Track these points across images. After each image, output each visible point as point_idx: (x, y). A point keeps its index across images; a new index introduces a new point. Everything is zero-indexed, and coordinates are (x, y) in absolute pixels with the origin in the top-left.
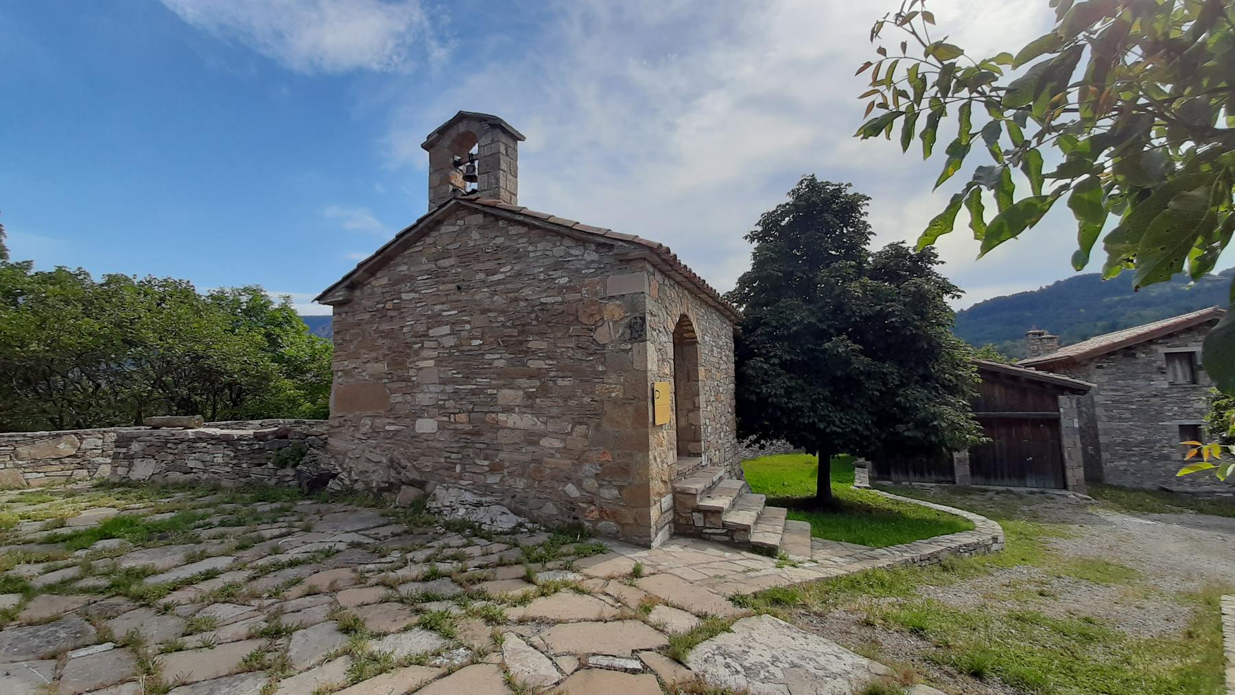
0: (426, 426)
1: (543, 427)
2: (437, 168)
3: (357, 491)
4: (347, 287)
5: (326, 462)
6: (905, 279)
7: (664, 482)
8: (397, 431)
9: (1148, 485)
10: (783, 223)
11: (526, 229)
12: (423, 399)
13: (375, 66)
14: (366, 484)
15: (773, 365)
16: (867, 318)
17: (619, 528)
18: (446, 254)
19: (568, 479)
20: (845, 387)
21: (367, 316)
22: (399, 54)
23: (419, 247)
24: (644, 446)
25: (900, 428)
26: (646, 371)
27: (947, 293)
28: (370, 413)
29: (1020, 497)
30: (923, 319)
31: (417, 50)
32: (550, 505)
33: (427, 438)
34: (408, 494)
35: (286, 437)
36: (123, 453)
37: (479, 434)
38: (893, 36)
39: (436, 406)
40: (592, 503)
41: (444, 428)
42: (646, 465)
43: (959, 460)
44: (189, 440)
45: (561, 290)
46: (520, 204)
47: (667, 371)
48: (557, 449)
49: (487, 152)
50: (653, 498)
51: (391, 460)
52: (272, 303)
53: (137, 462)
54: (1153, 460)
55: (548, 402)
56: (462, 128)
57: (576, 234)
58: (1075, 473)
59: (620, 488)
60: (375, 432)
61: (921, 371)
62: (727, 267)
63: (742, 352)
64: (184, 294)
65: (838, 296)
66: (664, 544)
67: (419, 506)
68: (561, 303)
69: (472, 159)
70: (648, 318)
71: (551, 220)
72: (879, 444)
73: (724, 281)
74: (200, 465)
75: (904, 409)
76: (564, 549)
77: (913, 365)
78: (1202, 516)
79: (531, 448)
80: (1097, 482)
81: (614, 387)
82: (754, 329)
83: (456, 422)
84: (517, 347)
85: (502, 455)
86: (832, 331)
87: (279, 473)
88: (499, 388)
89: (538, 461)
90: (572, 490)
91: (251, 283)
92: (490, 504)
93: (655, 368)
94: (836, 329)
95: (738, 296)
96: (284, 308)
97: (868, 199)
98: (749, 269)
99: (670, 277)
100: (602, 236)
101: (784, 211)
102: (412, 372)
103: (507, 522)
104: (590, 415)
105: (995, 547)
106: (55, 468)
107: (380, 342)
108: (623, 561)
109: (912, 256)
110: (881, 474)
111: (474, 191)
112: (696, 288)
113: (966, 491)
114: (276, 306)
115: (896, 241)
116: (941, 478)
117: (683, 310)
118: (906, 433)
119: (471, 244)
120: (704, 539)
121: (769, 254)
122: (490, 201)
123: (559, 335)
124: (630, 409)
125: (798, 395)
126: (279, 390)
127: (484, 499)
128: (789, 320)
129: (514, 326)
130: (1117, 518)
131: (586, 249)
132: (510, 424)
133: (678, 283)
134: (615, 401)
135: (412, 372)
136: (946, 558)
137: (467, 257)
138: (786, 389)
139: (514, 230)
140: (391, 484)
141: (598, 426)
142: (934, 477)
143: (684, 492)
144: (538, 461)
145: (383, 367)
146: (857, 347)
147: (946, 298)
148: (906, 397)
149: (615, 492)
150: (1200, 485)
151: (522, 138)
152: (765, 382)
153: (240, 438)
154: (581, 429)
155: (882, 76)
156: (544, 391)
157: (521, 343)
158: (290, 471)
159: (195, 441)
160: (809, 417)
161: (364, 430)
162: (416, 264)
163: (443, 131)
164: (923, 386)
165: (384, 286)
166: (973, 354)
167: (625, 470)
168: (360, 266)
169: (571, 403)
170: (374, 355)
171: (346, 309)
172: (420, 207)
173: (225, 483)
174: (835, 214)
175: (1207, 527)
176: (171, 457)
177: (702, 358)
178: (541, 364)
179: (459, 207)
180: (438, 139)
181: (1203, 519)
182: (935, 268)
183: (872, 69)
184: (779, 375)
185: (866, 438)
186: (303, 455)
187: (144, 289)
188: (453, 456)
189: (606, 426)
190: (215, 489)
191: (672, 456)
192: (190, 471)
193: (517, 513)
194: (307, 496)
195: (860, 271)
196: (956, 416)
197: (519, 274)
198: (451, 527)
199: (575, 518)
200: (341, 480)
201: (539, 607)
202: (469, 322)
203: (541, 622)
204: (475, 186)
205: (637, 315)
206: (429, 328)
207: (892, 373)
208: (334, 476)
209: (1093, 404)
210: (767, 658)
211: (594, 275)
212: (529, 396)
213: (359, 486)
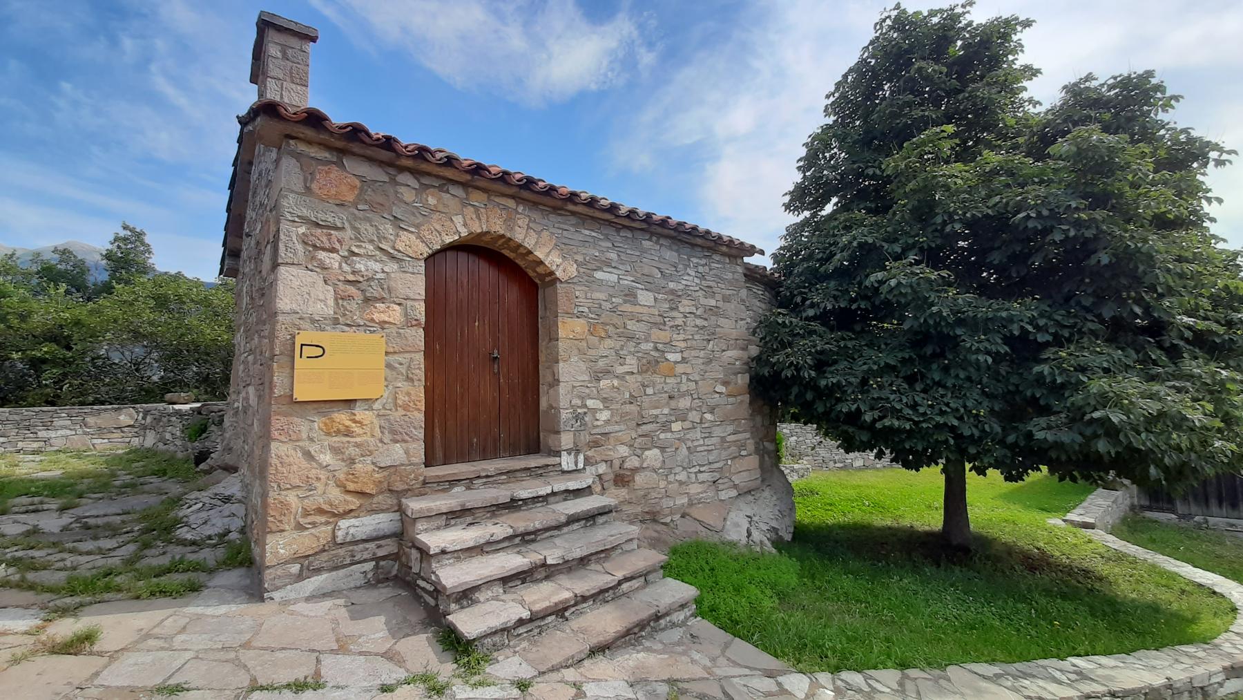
13: (593, 87)
22: (612, 70)
31: (627, 61)
61: (1107, 312)
106: (117, 435)
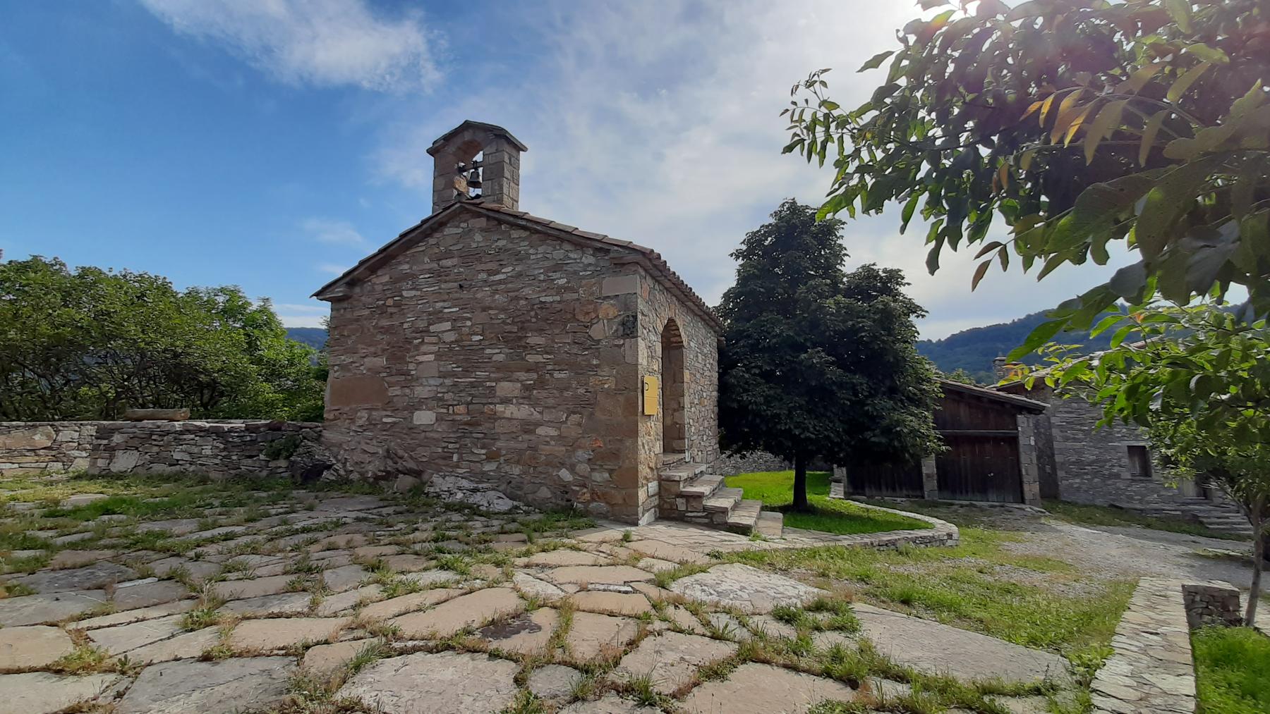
0: (424, 418)
1: (539, 416)
2: (443, 176)
3: (352, 482)
5: (320, 454)
6: (876, 297)
7: (651, 468)
8: (395, 423)
9: (1099, 502)
10: (766, 243)
12: (421, 392)
15: (755, 374)
16: (842, 334)
18: (448, 255)
19: (563, 465)
20: (820, 396)
21: (366, 312)
24: (634, 433)
25: (868, 434)
26: (636, 365)
28: (367, 406)
29: (982, 510)
30: (889, 335)
32: (544, 489)
33: (425, 429)
34: (406, 481)
35: (279, 429)
36: (103, 447)
37: (478, 424)
38: (803, 93)
39: (433, 398)
40: (584, 486)
42: (635, 451)
43: (928, 476)
44: (176, 432)
45: (560, 290)
46: (521, 210)
47: (656, 368)
48: (552, 437)
49: (491, 160)
50: (641, 481)
51: (388, 451)
52: (250, 304)
53: (119, 453)
54: (1105, 478)
55: (544, 394)
56: (467, 136)
58: (1032, 488)
59: (611, 471)
60: (372, 424)
62: (714, 278)
63: (726, 362)
64: (164, 289)
66: (649, 524)
67: (417, 491)
68: (559, 302)
69: (476, 165)
70: (640, 316)
73: (712, 299)
74: (187, 458)
76: (560, 524)
78: (1149, 530)
79: (527, 437)
80: (1052, 497)
81: (607, 379)
83: (454, 413)
84: (515, 342)
85: (499, 444)
88: (497, 380)
89: (534, 449)
90: (565, 475)
91: (229, 284)
92: (485, 490)
93: (645, 363)
95: (724, 311)
96: (263, 310)
98: (734, 284)
99: (659, 283)
101: (768, 230)
102: (411, 366)
103: (504, 505)
104: (584, 405)
105: (950, 542)
106: (31, 458)
107: (379, 337)
108: (616, 533)
110: (856, 488)
111: (478, 196)
113: (934, 505)
114: (254, 307)
116: (911, 493)
117: (671, 314)
121: (752, 270)
122: (494, 206)
123: (557, 331)
124: (621, 399)
126: (257, 393)
129: (513, 323)
130: (1066, 527)
131: (584, 253)
132: (508, 414)
134: (607, 393)
135: (411, 366)
136: (902, 546)
137: (470, 257)
138: (766, 398)
139: (515, 234)
140: (388, 473)
141: (592, 414)
142: (905, 492)
143: (669, 480)
144: (534, 449)
146: (831, 359)
149: (606, 475)
150: (1148, 503)
151: (524, 149)
152: (746, 391)
153: (231, 430)
155: (796, 118)
156: (541, 383)
157: (520, 338)
158: (283, 463)
159: (181, 433)
161: (360, 422)
162: (421, 261)
163: (448, 138)
164: (890, 399)
167: (615, 455)
168: (362, 263)
169: (566, 394)
170: (372, 349)
171: (345, 305)
172: (423, 209)
173: (213, 475)
174: (815, 236)
175: (1152, 539)
176: (155, 449)
178: (539, 358)
179: (463, 210)
180: (444, 146)
181: (1148, 532)
182: (902, 289)
183: (789, 113)
184: (758, 385)
186: (297, 446)
187: (120, 282)
188: (451, 446)
190: (204, 480)
191: (658, 447)
192: (177, 462)
194: (302, 486)
195: (835, 290)
196: (919, 424)
197: (520, 275)
198: (449, 508)
200: (336, 470)
201: (540, 558)
202: (470, 319)
203: (544, 567)
204: (479, 191)
208: (329, 467)
209: (1050, 426)
210: (736, 587)
211: (591, 276)
212: (527, 388)
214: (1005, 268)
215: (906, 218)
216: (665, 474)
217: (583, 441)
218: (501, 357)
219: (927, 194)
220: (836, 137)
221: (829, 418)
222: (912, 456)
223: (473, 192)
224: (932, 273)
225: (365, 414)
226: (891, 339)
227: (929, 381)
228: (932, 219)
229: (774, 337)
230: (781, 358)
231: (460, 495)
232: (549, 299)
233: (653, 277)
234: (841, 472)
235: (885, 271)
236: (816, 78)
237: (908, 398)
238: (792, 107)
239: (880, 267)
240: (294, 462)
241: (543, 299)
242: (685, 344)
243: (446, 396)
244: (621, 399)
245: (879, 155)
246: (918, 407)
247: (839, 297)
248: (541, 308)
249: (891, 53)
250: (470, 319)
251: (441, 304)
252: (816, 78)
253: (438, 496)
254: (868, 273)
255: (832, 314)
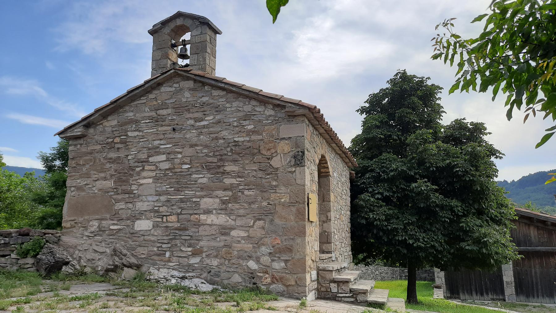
0: (143, 225)
1: (233, 223)
2: (158, 47)
4: (84, 126)
5: (61, 254)
8: (120, 230)
10: (384, 102)
11: (225, 93)
12: (141, 206)
14: (94, 268)
15: (378, 199)
16: (440, 170)
17: (285, 289)
18: (164, 106)
19: (250, 257)
20: (427, 215)
21: (98, 147)
23: (143, 100)
24: (302, 233)
25: (463, 244)
26: (304, 185)
27: (493, 155)
28: (97, 217)
30: (477, 170)
37: (185, 229)
38: (442, 30)
39: (151, 211)
40: (266, 272)
41: (158, 226)
48: (243, 238)
49: (198, 39)
50: (308, 269)
51: (115, 250)
55: (237, 206)
56: (179, 22)
57: (261, 97)
59: (286, 261)
60: (101, 230)
62: (348, 128)
63: (356, 191)
65: (421, 152)
68: (248, 141)
69: (184, 43)
70: (306, 152)
71: (243, 87)
72: (449, 256)
73: (347, 144)
75: (466, 232)
77: (471, 202)
79: (223, 238)
81: (283, 195)
82: (363, 175)
84: (216, 169)
85: (202, 243)
86: (417, 176)
87: (21, 262)
88: (202, 197)
90: (252, 265)
93: (309, 185)
94: (420, 175)
97: (441, 88)
98: (360, 132)
99: (316, 130)
100: (278, 100)
101: (384, 93)
102: (134, 187)
104: (266, 214)
107: (108, 166)
109: (469, 129)
111: (187, 65)
112: (330, 138)
115: (459, 118)
117: (323, 152)
118: (467, 247)
119: (184, 100)
120: (338, 301)
123: (247, 162)
124: (294, 209)
125: (395, 221)
127: (187, 275)
128: (388, 168)
129: (214, 156)
131: (266, 107)
132: (209, 222)
133: (320, 134)
134: (283, 205)
135: (134, 187)
137: (180, 109)
138: (386, 216)
139: (216, 93)
140: (116, 266)
141: (272, 220)
142: (490, 296)
145: (110, 184)
147: (493, 159)
148: (467, 223)
149: (283, 264)
154: (260, 223)
155: (439, 40)
156: (235, 199)
157: (219, 167)
158: (30, 260)
160: (402, 236)
161: (92, 229)
162: (143, 110)
163: (164, 23)
164: (479, 219)
165: (112, 127)
166: (516, 205)
167: (289, 250)
168: (97, 111)
169: (253, 206)
170: (103, 175)
171: (81, 141)
172: (143, 73)
174: (420, 98)
177: (332, 187)
178: (233, 181)
180: (161, 28)
182: (485, 138)
184: (381, 206)
185: (440, 252)
186: (42, 248)
188: (164, 246)
189: (277, 221)
193: (211, 283)
197: (219, 122)
199: (254, 284)
202: (181, 153)
204: (187, 61)
205: (299, 149)
206: (149, 156)
207: (457, 206)
208: (67, 263)
211: (271, 124)
212: (224, 202)
213: (88, 270)
214: (535, 116)
215: (495, 92)
216: (322, 266)
217: (266, 240)
218: (204, 180)
219: (505, 82)
220: (459, 53)
221: (434, 232)
222: (496, 261)
223: (182, 62)
224: (509, 119)
225: (96, 223)
226: (478, 173)
227: (507, 206)
228: (508, 94)
229: (392, 171)
230: (397, 187)
231: (173, 281)
232: (241, 139)
233: (313, 126)
234: (440, 276)
235: (472, 123)
236: (449, 22)
237: (491, 219)
238: (437, 37)
239: (468, 120)
240: (40, 260)
241: (236, 139)
242: (331, 173)
243: (161, 209)
244: (294, 209)
245: (482, 64)
246: (499, 225)
247: (439, 143)
248: (236, 145)
249: (486, 15)
250: (181, 153)
251: (158, 142)
252: (449, 22)
253: (158, 282)
254: (459, 125)
255: (435, 155)
